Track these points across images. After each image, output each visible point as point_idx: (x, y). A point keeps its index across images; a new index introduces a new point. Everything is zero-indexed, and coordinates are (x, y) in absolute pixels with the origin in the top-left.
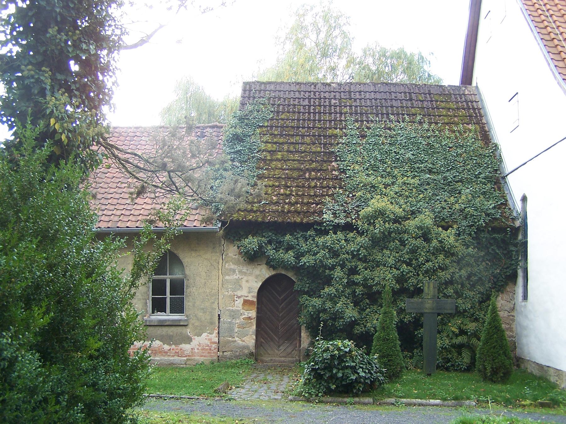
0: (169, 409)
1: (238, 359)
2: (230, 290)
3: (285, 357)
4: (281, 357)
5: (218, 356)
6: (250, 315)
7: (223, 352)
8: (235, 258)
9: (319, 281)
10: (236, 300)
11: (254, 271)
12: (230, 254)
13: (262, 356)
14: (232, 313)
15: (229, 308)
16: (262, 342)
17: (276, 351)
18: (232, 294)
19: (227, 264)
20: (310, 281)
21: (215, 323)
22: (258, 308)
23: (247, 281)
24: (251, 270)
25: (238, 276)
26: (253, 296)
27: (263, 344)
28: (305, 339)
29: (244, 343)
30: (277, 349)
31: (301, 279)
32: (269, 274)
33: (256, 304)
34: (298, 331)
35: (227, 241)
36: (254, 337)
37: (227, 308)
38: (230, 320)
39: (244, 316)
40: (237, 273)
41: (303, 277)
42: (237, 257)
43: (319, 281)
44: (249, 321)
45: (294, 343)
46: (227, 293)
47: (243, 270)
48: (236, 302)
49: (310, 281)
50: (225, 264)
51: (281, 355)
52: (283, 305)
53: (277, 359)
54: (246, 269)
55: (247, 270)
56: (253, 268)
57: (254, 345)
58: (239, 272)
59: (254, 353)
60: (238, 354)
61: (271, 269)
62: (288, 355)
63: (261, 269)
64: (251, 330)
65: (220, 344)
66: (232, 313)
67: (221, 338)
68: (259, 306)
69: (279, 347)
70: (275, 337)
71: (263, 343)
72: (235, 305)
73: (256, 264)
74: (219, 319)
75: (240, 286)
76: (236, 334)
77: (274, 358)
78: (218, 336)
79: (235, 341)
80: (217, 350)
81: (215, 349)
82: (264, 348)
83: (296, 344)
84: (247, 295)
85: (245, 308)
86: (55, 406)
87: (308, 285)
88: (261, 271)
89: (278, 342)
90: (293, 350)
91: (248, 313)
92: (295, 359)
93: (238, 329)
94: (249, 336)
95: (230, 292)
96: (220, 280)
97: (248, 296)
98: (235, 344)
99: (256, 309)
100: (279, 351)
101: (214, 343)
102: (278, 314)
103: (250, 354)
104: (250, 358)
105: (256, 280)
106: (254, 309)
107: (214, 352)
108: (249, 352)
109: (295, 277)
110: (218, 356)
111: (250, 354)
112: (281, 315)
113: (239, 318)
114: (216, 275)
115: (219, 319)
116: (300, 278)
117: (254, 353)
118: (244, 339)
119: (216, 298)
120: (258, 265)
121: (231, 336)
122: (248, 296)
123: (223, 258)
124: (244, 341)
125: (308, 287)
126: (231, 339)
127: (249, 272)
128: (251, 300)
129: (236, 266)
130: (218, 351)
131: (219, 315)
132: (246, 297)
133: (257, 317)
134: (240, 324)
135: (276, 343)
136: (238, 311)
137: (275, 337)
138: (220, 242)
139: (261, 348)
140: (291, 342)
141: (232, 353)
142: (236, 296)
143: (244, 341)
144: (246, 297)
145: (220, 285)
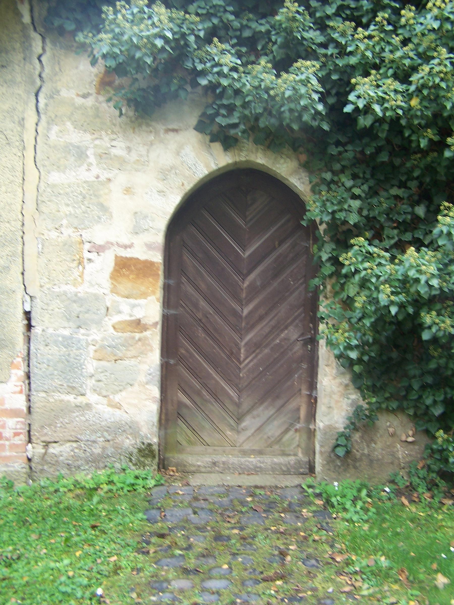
0: (25, 388)
1: (98, 468)
2: (65, 222)
3: (260, 453)
4: (245, 453)
5: (29, 460)
6: (139, 314)
7: (47, 444)
8: (82, 107)
9: (394, 191)
10: (89, 260)
11: (153, 155)
12: (64, 93)
13: (181, 451)
14: (76, 308)
15: (64, 288)
16: (180, 404)
17: (229, 433)
18: (75, 237)
19: (55, 129)
20: (365, 187)
21: (13, 345)
22: (167, 289)
23: (128, 191)
24: (142, 150)
25: (95, 170)
26: (150, 246)
27: (184, 412)
28: (336, 397)
29: (118, 413)
30: (232, 429)
31: (332, 181)
32: (207, 166)
33: (161, 273)
34: (305, 366)
35: (54, 43)
36: (156, 392)
37: (57, 289)
38: (66, 332)
39: (117, 318)
40: (92, 159)
41: (334, 173)
42: (90, 102)
43: (394, 191)
44: (137, 336)
45: (292, 405)
46: (54, 234)
47: (114, 151)
48: (89, 267)
49: (365, 187)
50: (49, 129)
51: (246, 447)
52: (252, 276)
53: (233, 460)
54: (123, 145)
55: (129, 149)
56: (152, 144)
57: (155, 419)
58: (100, 156)
59: (155, 448)
60: (97, 450)
61: (217, 147)
62: (270, 446)
63: (181, 147)
64: (145, 367)
65: (35, 416)
66: (76, 308)
67: (37, 397)
68: (171, 282)
69: (239, 419)
70: (227, 388)
71: (186, 406)
72: (86, 277)
73: (161, 127)
74: (29, 327)
75: (104, 208)
76: (91, 383)
77: (224, 459)
78: (25, 388)
79: (88, 406)
80: (23, 438)
81: (16, 434)
82: (189, 426)
83: (298, 409)
84: (127, 242)
85: (121, 288)
86: (436, 66)
87: (356, 204)
88: (178, 153)
89: (238, 405)
90: (287, 431)
91: (133, 306)
92: (292, 459)
93: (95, 363)
94: (136, 387)
95: (68, 232)
96: (30, 187)
97: (131, 246)
98: (89, 415)
99: (159, 293)
100: (238, 432)
101: (14, 413)
102: (238, 308)
103: (140, 450)
104: (140, 464)
105: (160, 186)
106: (154, 293)
107: (13, 447)
108: (139, 445)
109: (304, 176)
110: (29, 460)
111: (140, 450)
112: (246, 312)
113: (99, 323)
114: (13, 169)
115: (29, 327)
116: (328, 176)
117: (155, 448)
118: (117, 398)
119: (14, 254)
120: (168, 131)
121: (72, 389)
122: (131, 246)
123: (41, 105)
124: (118, 406)
125: (360, 211)
126: (70, 398)
127: (134, 156)
128: (142, 257)
129: (88, 137)
130: (30, 441)
131: (28, 315)
132: (126, 247)
133: (166, 319)
134: (103, 347)
135: (231, 407)
136: (96, 297)
137: (227, 388)
138: (27, 38)
139: (180, 422)
140: (279, 403)
141: (79, 448)
142: (87, 246)
143: (118, 406)
144: (126, 247)
145: (30, 206)
